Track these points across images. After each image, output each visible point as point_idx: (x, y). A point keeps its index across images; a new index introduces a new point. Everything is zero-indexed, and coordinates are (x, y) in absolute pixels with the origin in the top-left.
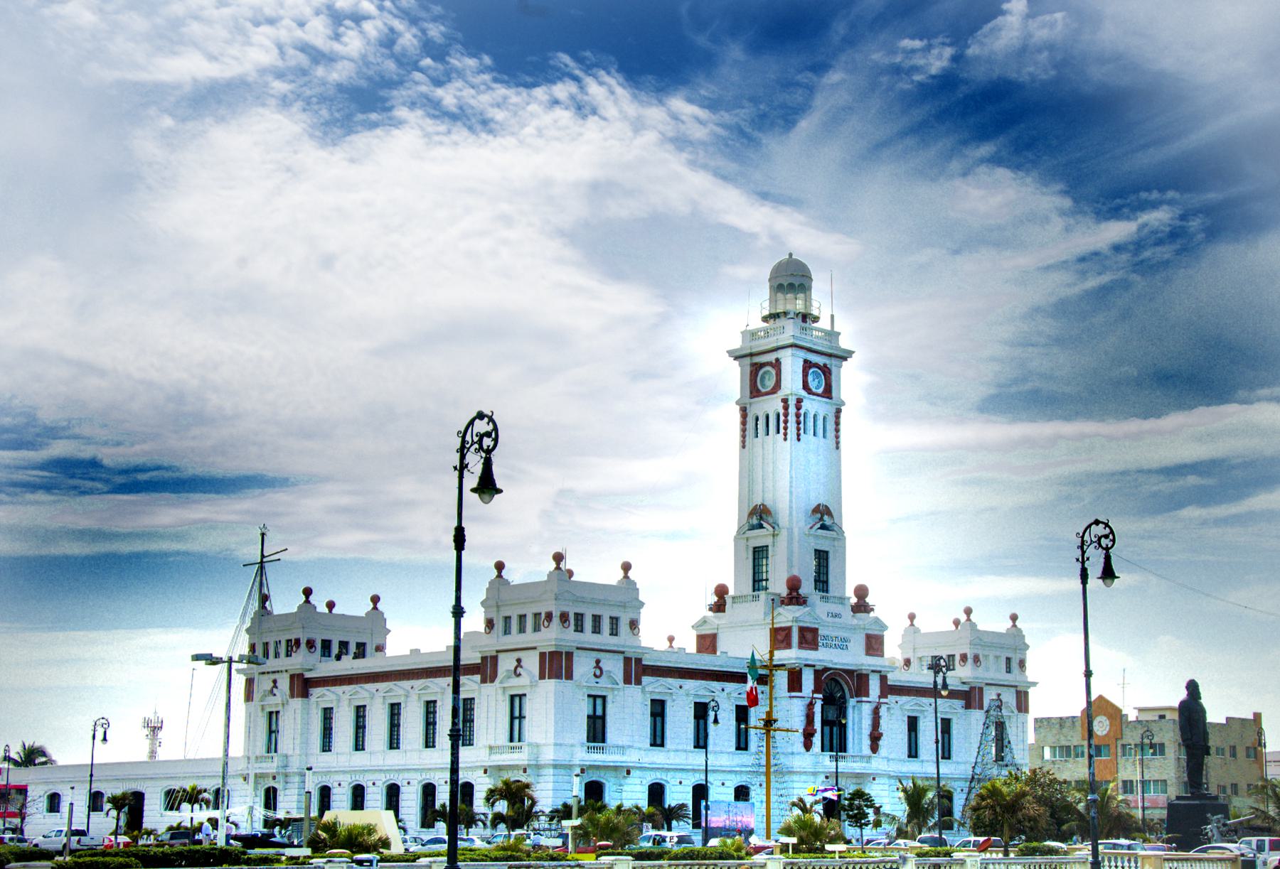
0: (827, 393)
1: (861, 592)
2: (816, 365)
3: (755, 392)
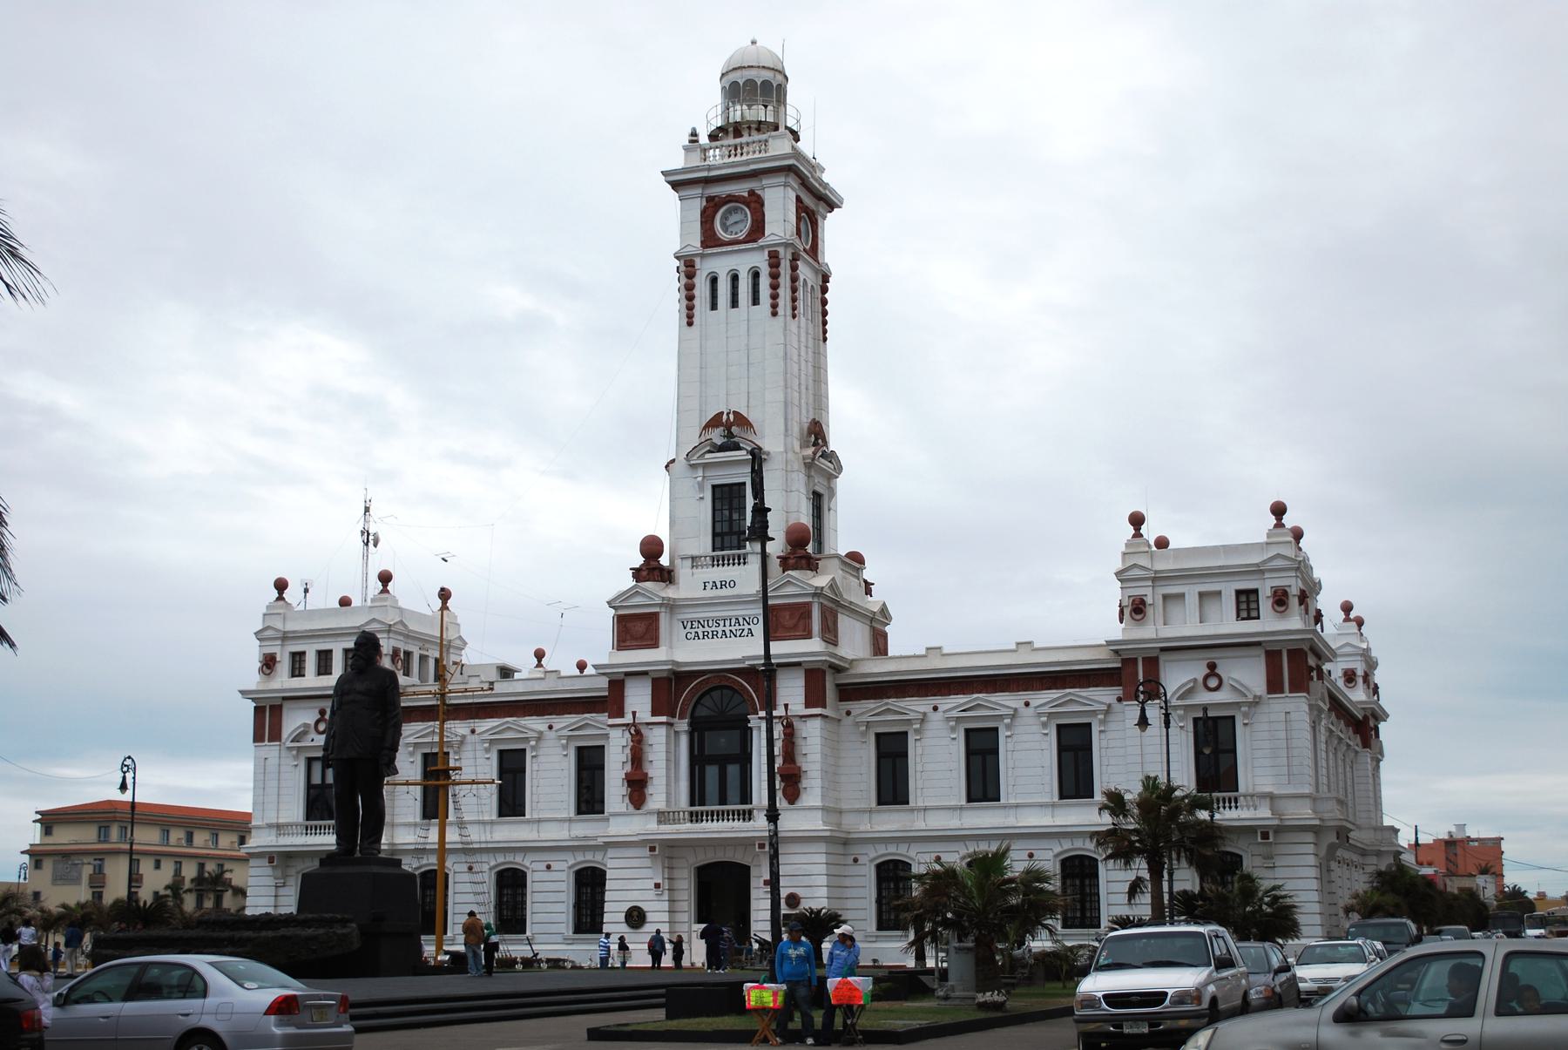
3: (710, 239)
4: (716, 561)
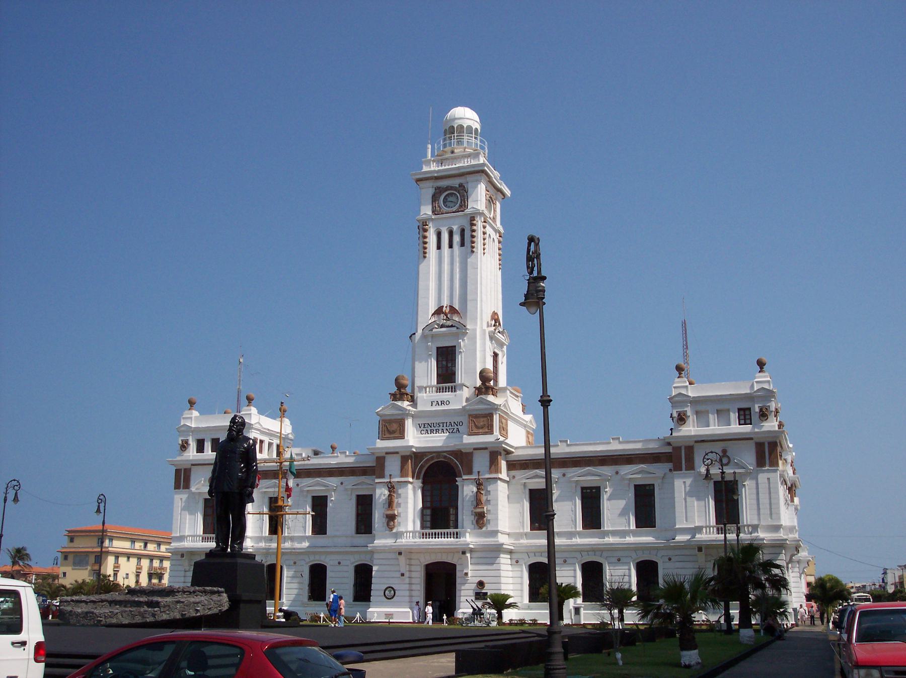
4: (439, 390)
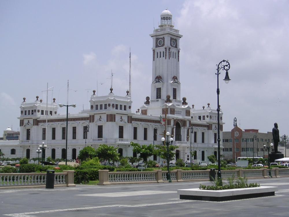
0: (176, 47)
1: (184, 99)
2: (173, 39)
3: (157, 46)
